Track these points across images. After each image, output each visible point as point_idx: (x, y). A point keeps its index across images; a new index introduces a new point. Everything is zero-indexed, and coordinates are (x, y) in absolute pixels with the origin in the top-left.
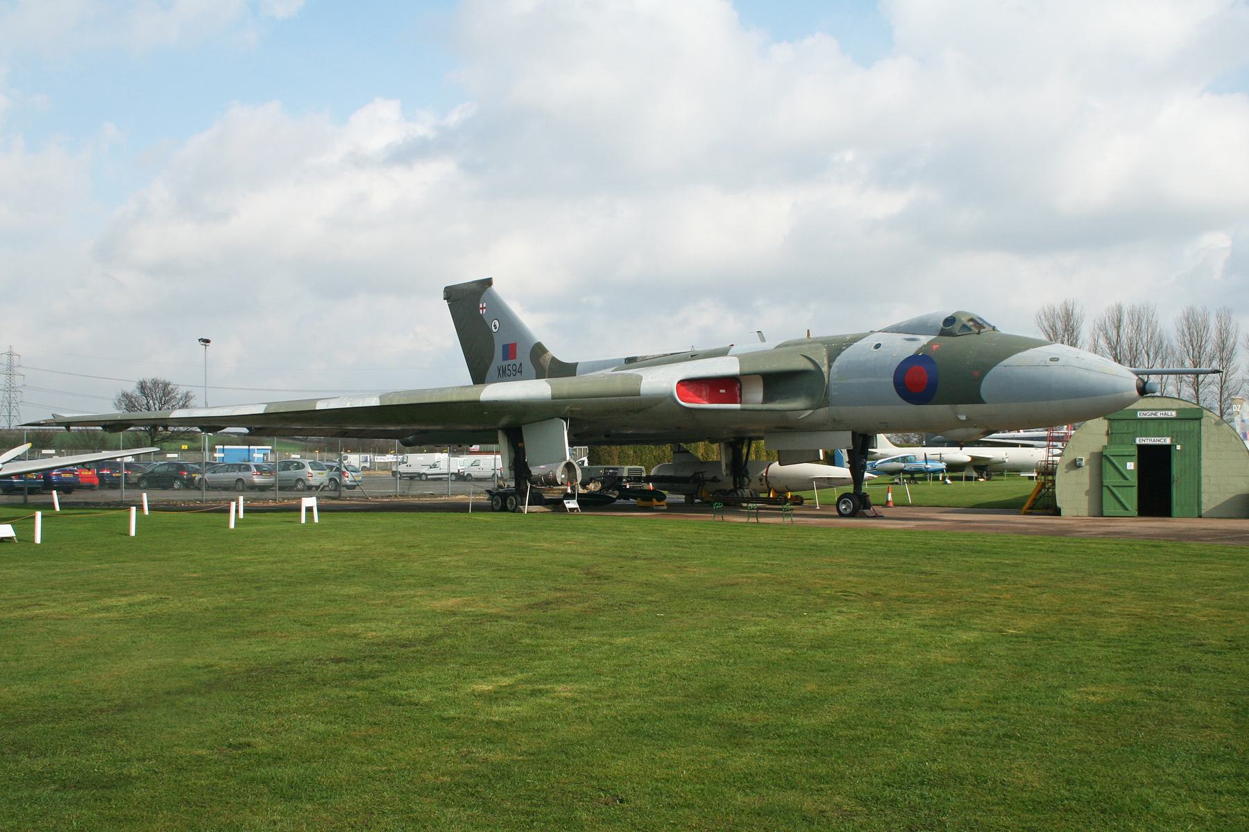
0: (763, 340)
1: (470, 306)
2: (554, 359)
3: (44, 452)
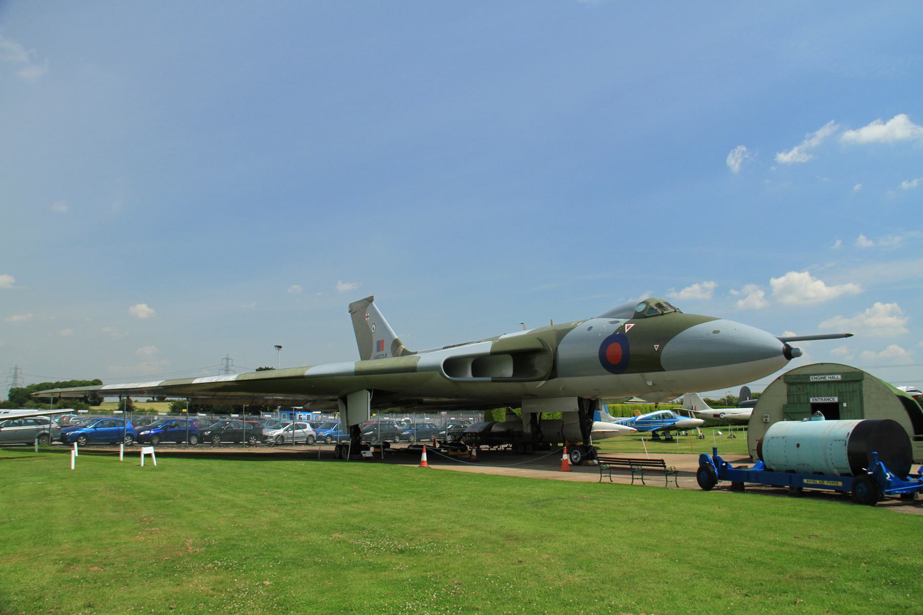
1: (361, 311)
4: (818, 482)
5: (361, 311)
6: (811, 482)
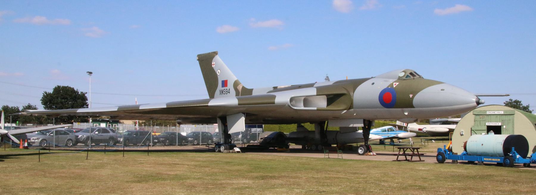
1: (206, 62)
4: (490, 159)
5: (206, 62)
6: (487, 159)
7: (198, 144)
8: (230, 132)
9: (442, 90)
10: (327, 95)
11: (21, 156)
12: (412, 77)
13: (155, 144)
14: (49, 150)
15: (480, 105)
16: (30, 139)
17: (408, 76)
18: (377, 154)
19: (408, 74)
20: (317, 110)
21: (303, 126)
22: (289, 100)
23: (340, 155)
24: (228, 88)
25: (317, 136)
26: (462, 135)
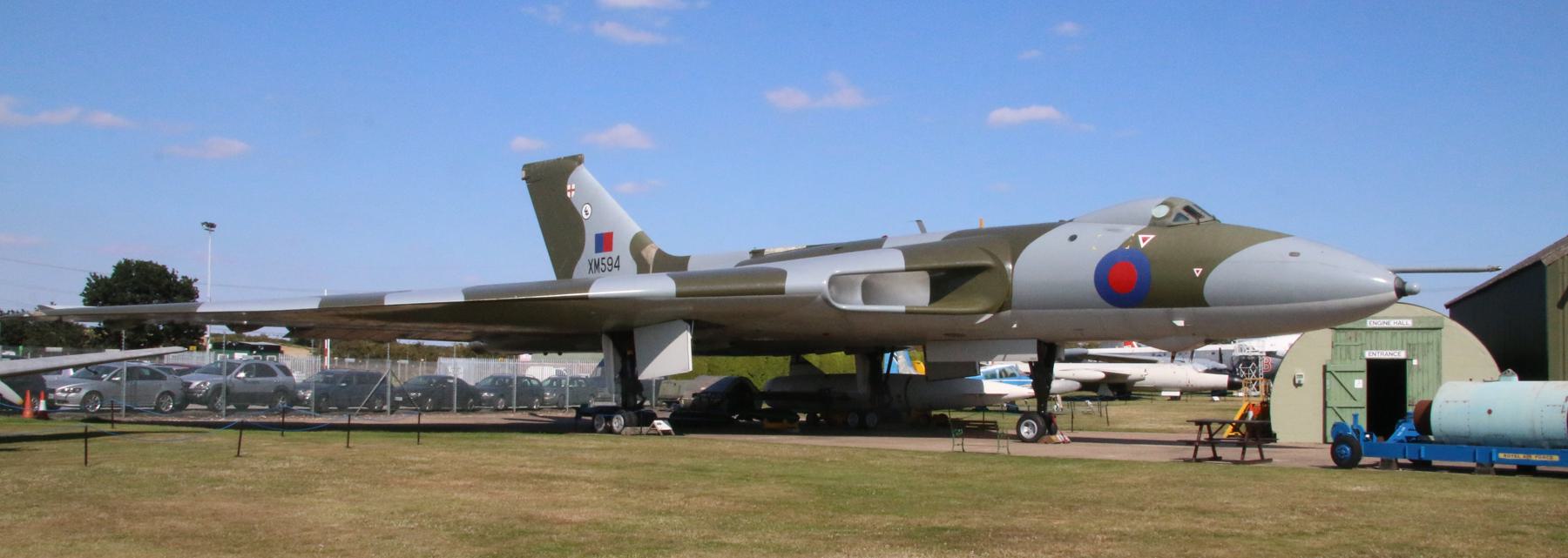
0: (923, 230)
1: (548, 184)
2: (659, 252)
3: (49, 349)
5: (548, 184)
7: (506, 409)
8: (643, 376)
9: (1292, 254)
10: (931, 271)
11: (25, 445)
12: (1192, 219)
13: (395, 408)
14: (112, 422)
15: (1404, 299)
16: (53, 391)
17: (1179, 216)
18: (1074, 440)
19: (1179, 209)
20: (907, 312)
21: (807, 363)
22: (825, 282)
23: (959, 441)
24: (613, 254)
25: (862, 389)
26: (1298, 385)
